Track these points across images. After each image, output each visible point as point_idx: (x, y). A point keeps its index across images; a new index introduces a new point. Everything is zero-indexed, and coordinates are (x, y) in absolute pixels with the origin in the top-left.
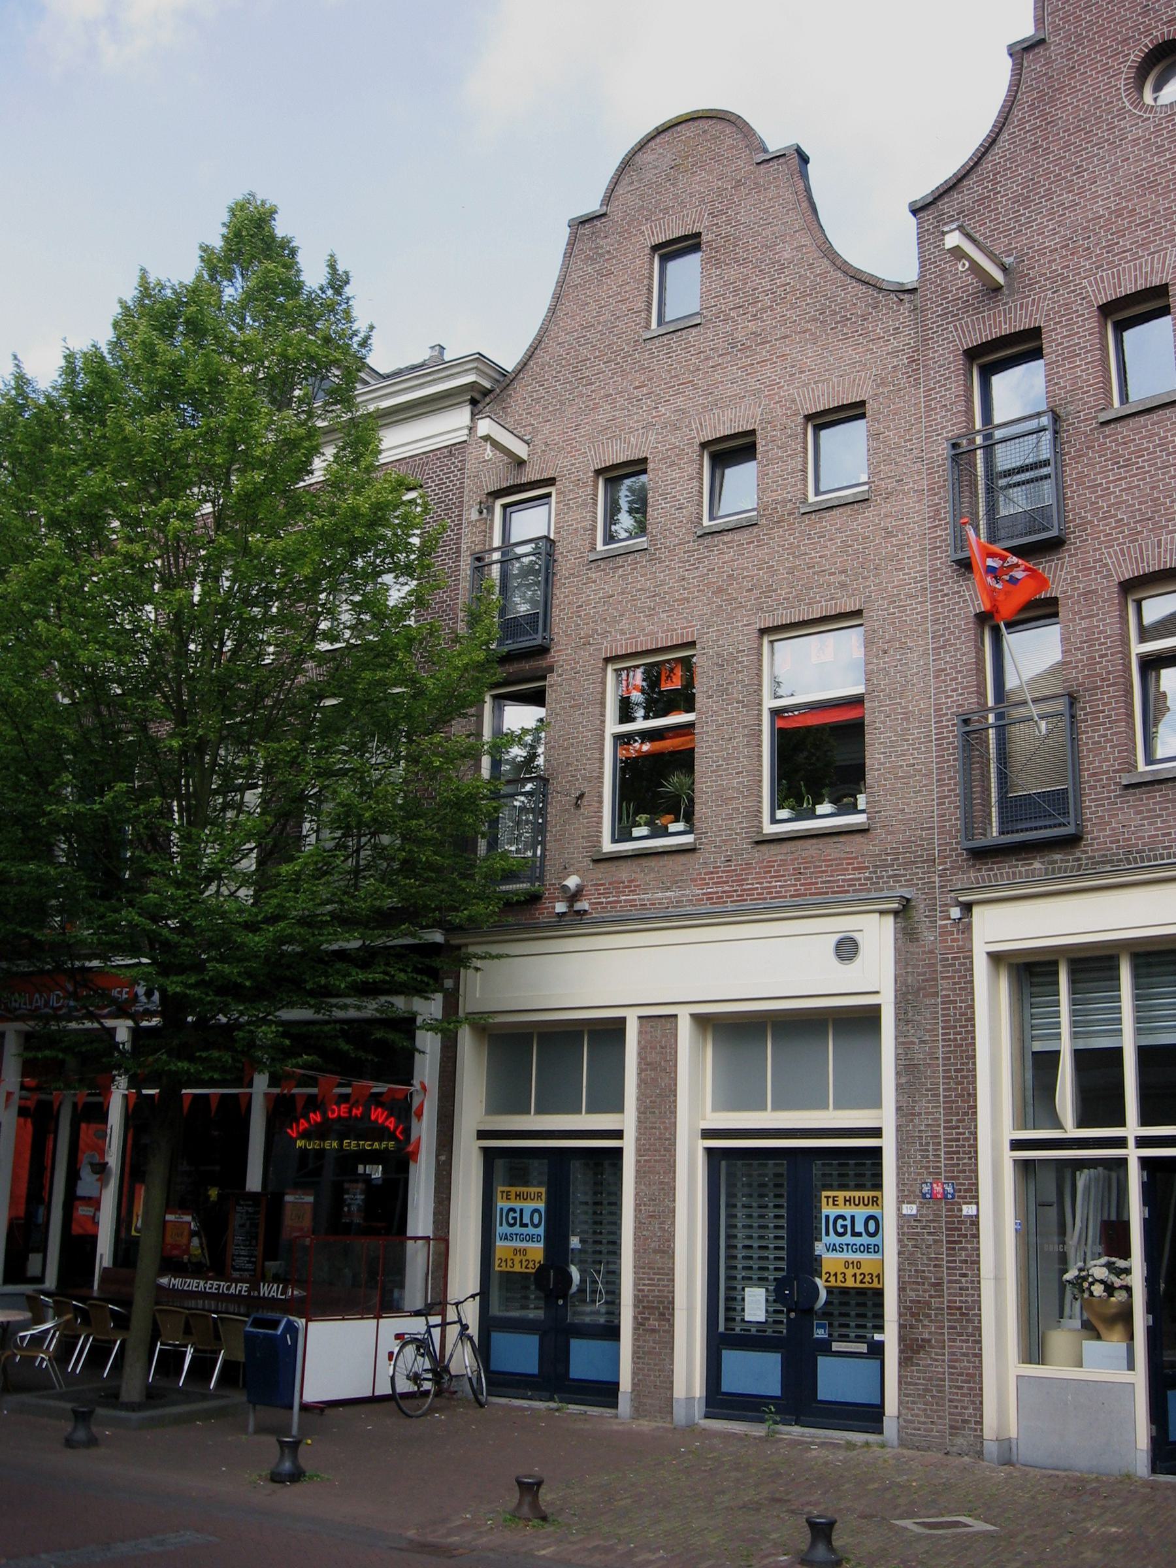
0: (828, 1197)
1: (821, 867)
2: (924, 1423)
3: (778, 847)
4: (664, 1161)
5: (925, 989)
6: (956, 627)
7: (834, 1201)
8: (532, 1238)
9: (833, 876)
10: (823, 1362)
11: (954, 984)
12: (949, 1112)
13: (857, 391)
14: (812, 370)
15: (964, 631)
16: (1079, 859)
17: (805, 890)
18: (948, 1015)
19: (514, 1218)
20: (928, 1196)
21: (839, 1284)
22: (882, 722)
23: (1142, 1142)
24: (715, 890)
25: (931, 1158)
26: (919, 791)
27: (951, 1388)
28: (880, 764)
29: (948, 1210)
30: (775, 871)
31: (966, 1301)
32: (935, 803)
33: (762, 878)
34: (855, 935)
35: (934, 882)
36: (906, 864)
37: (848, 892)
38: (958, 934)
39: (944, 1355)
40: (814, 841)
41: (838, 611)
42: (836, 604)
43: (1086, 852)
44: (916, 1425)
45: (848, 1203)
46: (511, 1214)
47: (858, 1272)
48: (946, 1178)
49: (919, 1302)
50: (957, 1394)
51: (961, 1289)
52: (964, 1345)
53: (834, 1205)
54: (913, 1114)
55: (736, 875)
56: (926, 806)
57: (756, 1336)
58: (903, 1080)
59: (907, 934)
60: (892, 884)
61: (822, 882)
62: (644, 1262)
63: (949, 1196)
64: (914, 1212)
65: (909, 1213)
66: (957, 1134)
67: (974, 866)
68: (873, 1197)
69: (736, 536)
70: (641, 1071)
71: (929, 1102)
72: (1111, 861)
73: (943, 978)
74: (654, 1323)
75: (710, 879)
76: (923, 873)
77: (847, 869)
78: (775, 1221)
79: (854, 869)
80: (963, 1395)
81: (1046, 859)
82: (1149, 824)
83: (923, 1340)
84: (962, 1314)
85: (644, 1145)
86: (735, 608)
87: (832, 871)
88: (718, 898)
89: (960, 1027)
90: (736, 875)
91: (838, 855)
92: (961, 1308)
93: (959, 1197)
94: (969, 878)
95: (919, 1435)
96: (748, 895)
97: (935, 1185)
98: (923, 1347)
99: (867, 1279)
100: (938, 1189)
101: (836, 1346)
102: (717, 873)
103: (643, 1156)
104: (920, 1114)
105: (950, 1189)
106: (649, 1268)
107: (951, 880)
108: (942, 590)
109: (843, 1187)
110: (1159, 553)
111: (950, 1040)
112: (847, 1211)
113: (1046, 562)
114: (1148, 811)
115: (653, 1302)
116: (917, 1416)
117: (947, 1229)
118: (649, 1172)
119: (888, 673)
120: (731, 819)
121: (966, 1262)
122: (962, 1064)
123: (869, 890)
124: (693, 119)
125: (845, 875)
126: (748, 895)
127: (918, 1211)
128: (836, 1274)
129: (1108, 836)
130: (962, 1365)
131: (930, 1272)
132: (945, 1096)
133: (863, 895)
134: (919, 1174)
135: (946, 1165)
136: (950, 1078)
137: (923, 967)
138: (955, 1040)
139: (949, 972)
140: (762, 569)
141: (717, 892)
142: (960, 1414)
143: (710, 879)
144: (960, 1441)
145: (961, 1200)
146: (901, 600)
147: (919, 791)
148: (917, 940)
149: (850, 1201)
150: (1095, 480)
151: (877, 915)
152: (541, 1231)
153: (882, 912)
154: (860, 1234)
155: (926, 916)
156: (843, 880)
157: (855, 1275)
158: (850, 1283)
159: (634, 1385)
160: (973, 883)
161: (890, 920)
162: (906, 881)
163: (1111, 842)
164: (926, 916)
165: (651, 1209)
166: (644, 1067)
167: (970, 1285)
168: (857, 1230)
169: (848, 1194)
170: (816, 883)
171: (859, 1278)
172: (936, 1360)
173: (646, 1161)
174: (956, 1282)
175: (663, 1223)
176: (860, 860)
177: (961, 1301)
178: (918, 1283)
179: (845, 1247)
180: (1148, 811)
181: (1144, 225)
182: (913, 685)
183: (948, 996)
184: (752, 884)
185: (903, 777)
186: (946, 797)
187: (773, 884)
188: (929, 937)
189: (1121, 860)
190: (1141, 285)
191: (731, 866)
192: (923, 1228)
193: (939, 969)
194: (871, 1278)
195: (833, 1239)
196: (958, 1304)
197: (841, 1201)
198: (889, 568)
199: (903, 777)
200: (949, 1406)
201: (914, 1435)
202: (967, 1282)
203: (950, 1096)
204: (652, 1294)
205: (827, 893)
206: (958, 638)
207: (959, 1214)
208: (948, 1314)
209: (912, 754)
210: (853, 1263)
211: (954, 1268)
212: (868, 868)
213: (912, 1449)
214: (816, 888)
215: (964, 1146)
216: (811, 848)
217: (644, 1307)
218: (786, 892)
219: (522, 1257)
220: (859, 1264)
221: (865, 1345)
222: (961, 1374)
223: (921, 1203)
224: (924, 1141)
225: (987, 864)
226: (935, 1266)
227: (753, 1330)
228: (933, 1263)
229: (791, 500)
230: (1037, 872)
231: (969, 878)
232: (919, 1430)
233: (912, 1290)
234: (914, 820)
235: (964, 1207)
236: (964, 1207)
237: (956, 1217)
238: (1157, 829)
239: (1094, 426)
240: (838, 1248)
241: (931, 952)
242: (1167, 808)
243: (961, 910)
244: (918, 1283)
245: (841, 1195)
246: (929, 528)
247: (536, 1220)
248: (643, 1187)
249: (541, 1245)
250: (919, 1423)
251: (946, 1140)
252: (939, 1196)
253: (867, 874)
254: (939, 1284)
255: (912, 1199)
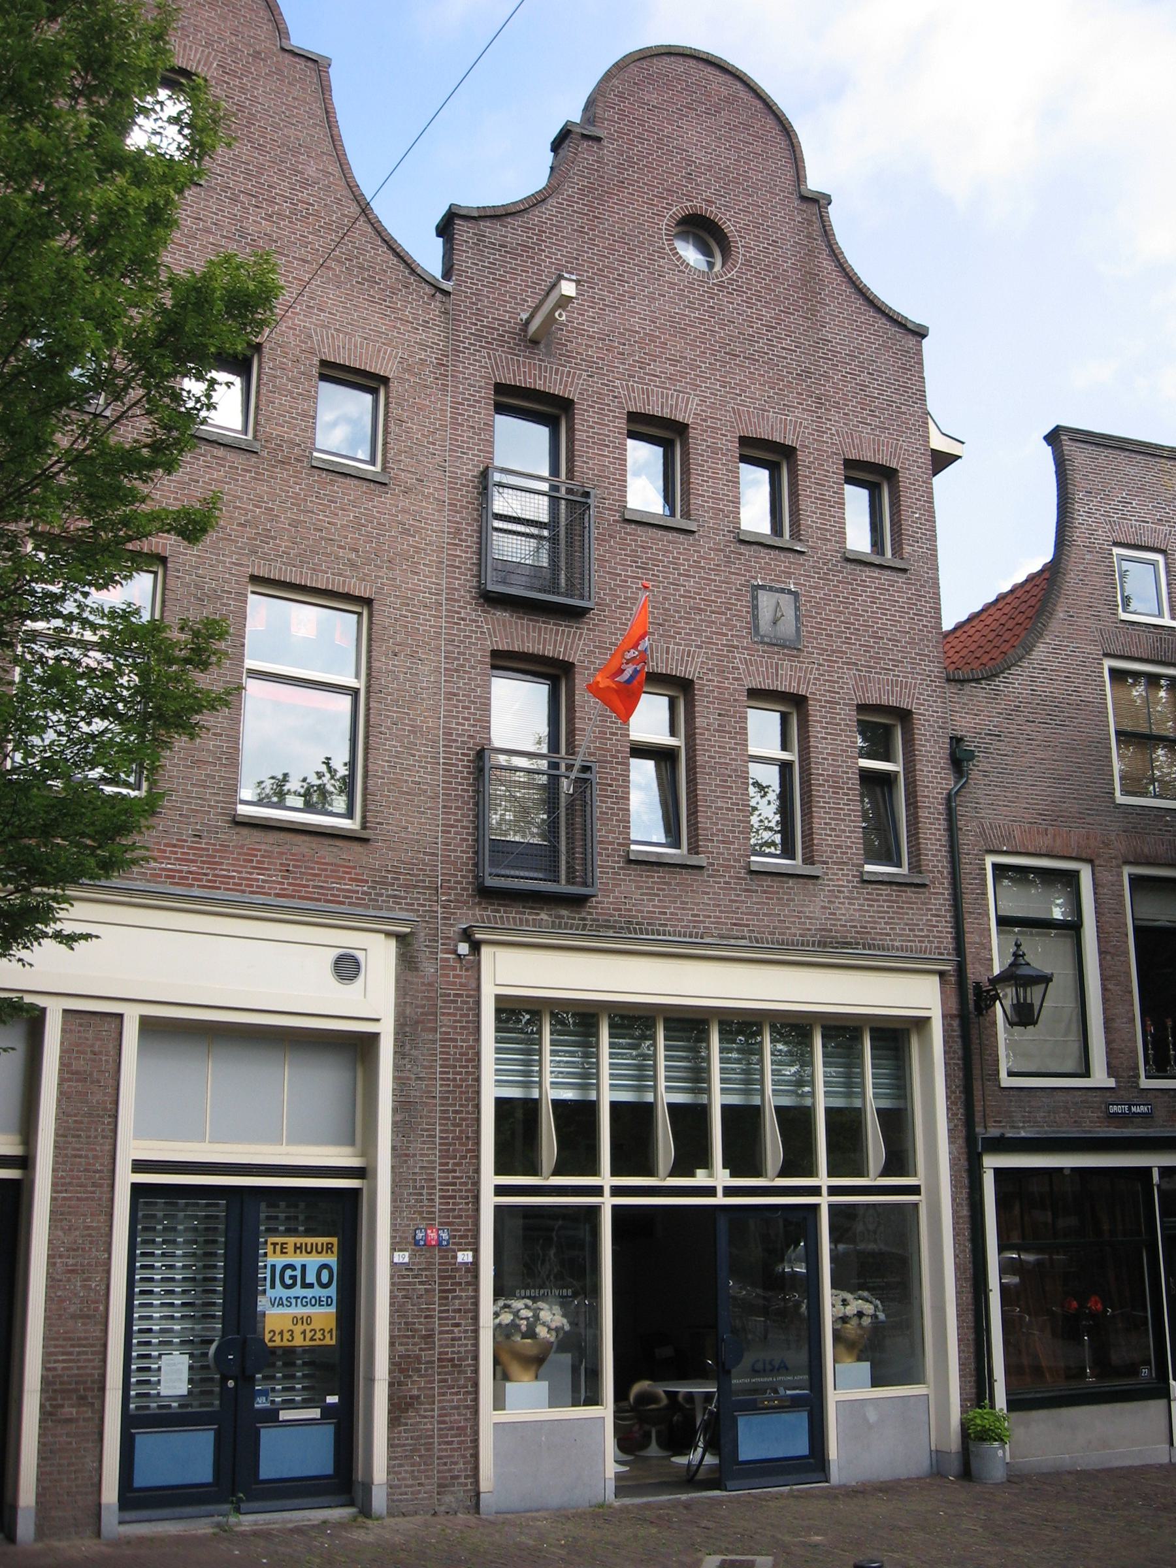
0: (275, 1244)
1: (313, 868)
2: (411, 1486)
3: (263, 834)
4: (93, 1199)
5: (423, 1022)
6: (471, 655)
7: (282, 1248)
8: (318, 1302)
9: (326, 882)
10: (268, 1436)
11: (455, 1021)
12: (445, 1154)
13: (382, 365)
14: (333, 314)
15: (480, 662)
16: (584, 919)
17: (294, 891)
18: (448, 1053)
19: (293, 1278)
20: (422, 1243)
21: (285, 1343)
22: (389, 728)
23: (617, 1191)
24: (178, 867)
25: (426, 1203)
26: (423, 813)
27: (439, 1445)
28: (385, 772)
29: (441, 1258)
30: (258, 862)
31: (459, 1352)
32: (440, 829)
33: (241, 866)
34: (360, 955)
35: (437, 912)
36: (407, 886)
37: (343, 903)
38: (461, 970)
39: (433, 1410)
40: (307, 838)
41: (346, 590)
42: (344, 582)
43: (591, 914)
44: (404, 1489)
45: (298, 1251)
46: (289, 1272)
47: (308, 1328)
48: (441, 1224)
49: (409, 1356)
50: (446, 1450)
51: (453, 1339)
52: (456, 1398)
53: (282, 1252)
54: (407, 1155)
55: (207, 856)
56: (430, 830)
57: (136, 1415)
58: (398, 1118)
59: (407, 961)
60: (391, 905)
61: (315, 887)
62: (58, 1332)
63: (445, 1243)
64: (406, 1260)
65: (401, 1261)
66: (454, 1178)
67: (479, 903)
68: (327, 1244)
69: (231, 456)
70: (62, 1081)
71: (424, 1143)
72: (615, 927)
73: (443, 1014)
74: (69, 1411)
75: (171, 852)
76: (425, 900)
77: (344, 878)
78: (203, 1271)
79: (351, 879)
80: (453, 1450)
81: (553, 912)
82: (648, 900)
83: (411, 1397)
84: (454, 1366)
85: (62, 1177)
86: (222, 539)
87: (326, 876)
88: (181, 878)
89: (461, 1067)
90: (207, 856)
91: (334, 861)
92: (452, 1360)
93: (454, 1244)
94: (474, 915)
95: (407, 1500)
96: (221, 883)
97: (429, 1231)
98: (410, 1405)
99: (319, 1335)
100: (433, 1235)
101: (284, 1415)
102: (182, 847)
103: (61, 1192)
104: (415, 1155)
105: (445, 1236)
106: (65, 1339)
107: (455, 913)
108: (459, 613)
109: (291, 1232)
110: (667, 658)
111: (448, 1079)
112: (298, 1260)
113: (566, 626)
114: (648, 888)
115: (70, 1383)
116: (404, 1479)
117: (441, 1277)
118: (69, 1213)
119: (397, 678)
120: (205, 787)
121: (459, 1311)
122: (461, 1105)
123: (367, 906)
124: (669, 54)
125: (340, 884)
126: (221, 883)
127: (410, 1259)
128: (281, 1333)
129: (611, 903)
130: (453, 1418)
131: (420, 1323)
132: (441, 1138)
133: (359, 911)
134: (412, 1219)
135: (440, 1211)
136: (448, 1119)
137: (422, 999)
138: (455, 1080)
139: (450, 1008)
140: (260, 507)
141: (181, 871)
142: (450, 1471)
143: (171, 852)
144: (448, 1498)
145: (456, 1247)
146: (414, 606)
147: (423, 813)
148: (417, 969)
149: (300, 1248)
150: (616, 569)
151: (382, 936)
152: (332, 1291)
153: (388, 934)
154: (311, 1286)
155: (426, 946)
156: (339, 890)
157: (304, 1332)
158: (298, 1341)
159: (38, 1495)
160: (478, 922)
161: (392, 944)
162: (406, 904)
163: (614, 910)
164: (426, 946)
165: (71, 1261)
166: (66, 1076)
167: (463, 1335)
168: (308, 1281)
169: (300, 1240)
170: (308, 886)
171: (309, 1335)
172: (425, 1417)
173: (64, 1199)
174: (447, 1332)
175: (88, 1279)
176: (357, 871)
177: (453, 1352)
178: (408, 1337)
179: (293, 1301)
180: (648, 888)
181: (674, 362)
182: (422, 699)
183: (448, 1033)
184: (228, 871)
185: (408, 793)
186: (452, 826)
187: (254, 876)
188: (428, 968)
189: (622, 928)
190: (666, 413)
191: (201, 843)
192: (415, 1277)
193: (440, 1004)
194: (323, 1334)
195: (280, 1291)
196: (450, 1356)
197: (291, 1249)
198: (404, 567)
199: (408, 793)
200: (438, 1464)
201: (400, 1501)
202: (460, 1332)
203: (447, 1138)
204: (68, 1372)
205: (319, 900)
206: (473, 667)
207: (453, 1261)
208: (439, 1367)
209: (418, 772)
210: (302, 1318)
211: (447, 1318)
212: (367, 881)
213: (398, 1516)
214: (306, 892)
215: (461, 1191)
216: (303, 845)
217: (55, 1391)
218: (270, 888)
219: (305, 1326)
220: (308, 1319)
221: (319, 1410)
222: (452, 1429)
223: (413, 1250)
224: (418, 1185)
225: (493, 904)
226: (426, 1317)
227: (175, 1404)
228: (423, 1314)
229: (299, 445)
230: (543, 922)
231: (474, 915)
232: (406, 1494)
233: (401, 1344)
234: (418, 841)
235: (460, 1254)
236: (460, 1254)
237: (450, 1264)
238: (654, 906)
239: (617, 518)
240: (285, 1302)
241: (431, 984)
242: (664, 890)
243: (470, 947)
244: (408, 1337)
245: (291, 1241)
246: (448, 544)
247: (325, 1278)
248: (60, 1233)
249: (332, 1310)
250: (406, 1486)
251: (441, 1184)
252: (433, 1243)
253: (365, 888)
254: (431, 1336)
255: (403, 1246)
